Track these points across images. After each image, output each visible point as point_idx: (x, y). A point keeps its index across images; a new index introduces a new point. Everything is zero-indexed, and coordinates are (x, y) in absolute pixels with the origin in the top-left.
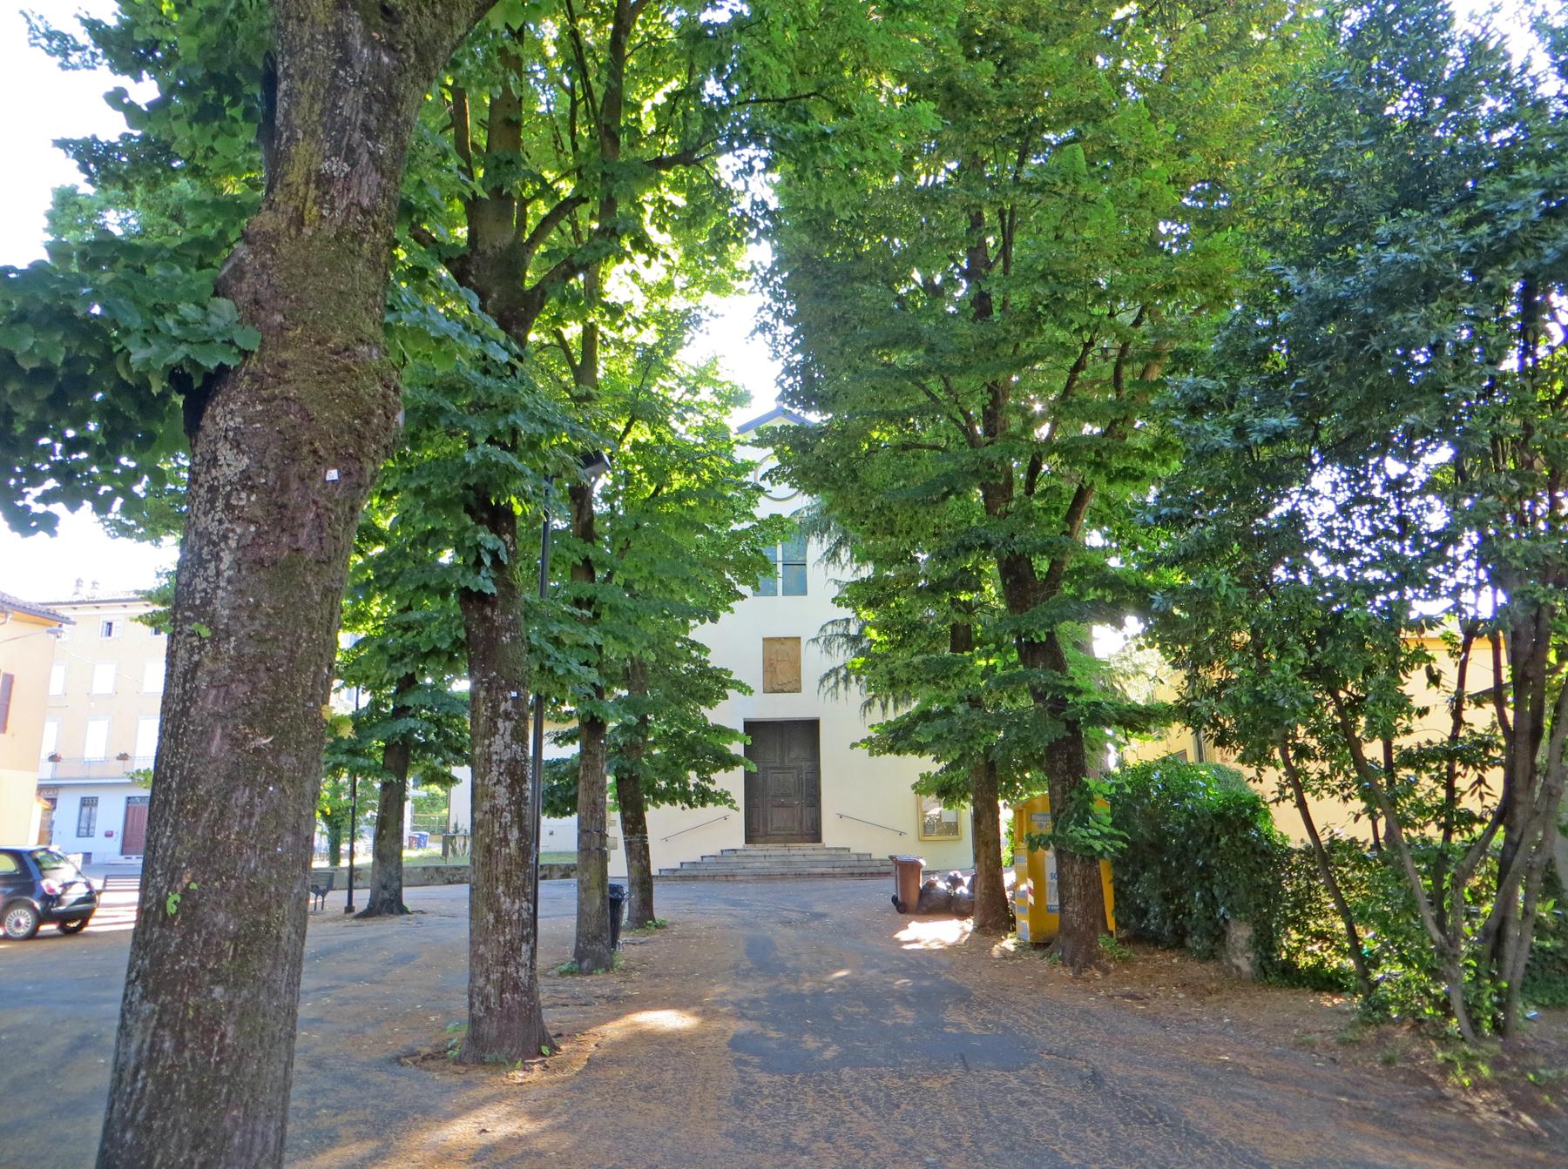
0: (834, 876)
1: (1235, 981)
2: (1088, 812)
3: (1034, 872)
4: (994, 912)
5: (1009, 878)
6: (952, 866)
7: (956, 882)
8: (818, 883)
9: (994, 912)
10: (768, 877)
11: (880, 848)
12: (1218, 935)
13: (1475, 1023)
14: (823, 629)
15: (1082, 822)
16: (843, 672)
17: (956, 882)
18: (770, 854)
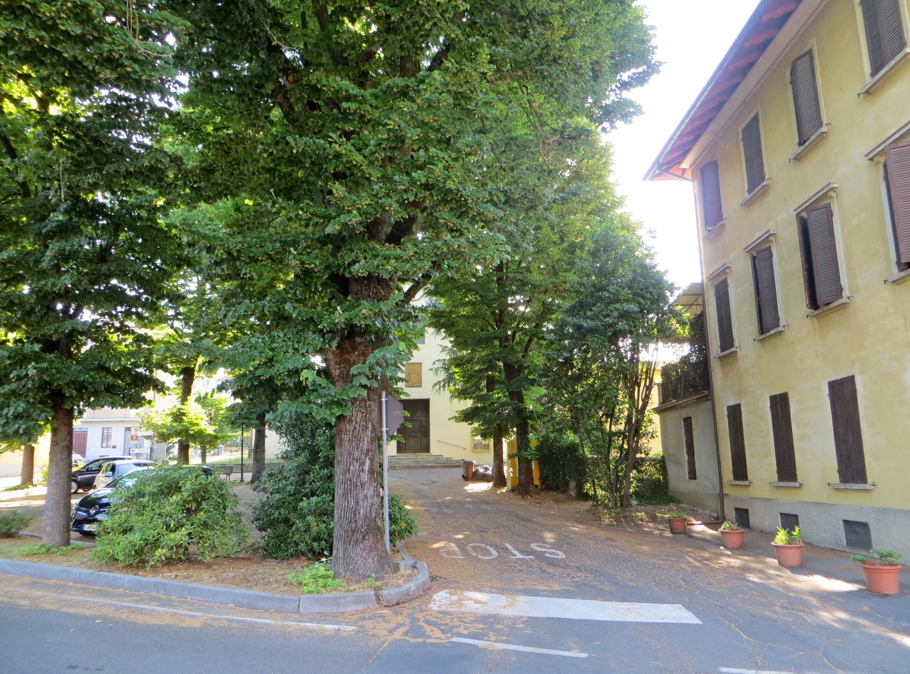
0: (436, 467)
1: (571, 499)
2: (528, 446)
3: (513, 466)
4: (500, 480)
5: (505, 468)
6: (484, 462)
7: (487, 469)
8: (430, 470)
9: (500, 480)
10: (409, 468)
11: (457, 455)
12: (567, 485)
13: (616, 504)
14: (434, 363)
15: (526, 450)
16: (442, 383)
17: (487, 469)
18: (408, 458)
